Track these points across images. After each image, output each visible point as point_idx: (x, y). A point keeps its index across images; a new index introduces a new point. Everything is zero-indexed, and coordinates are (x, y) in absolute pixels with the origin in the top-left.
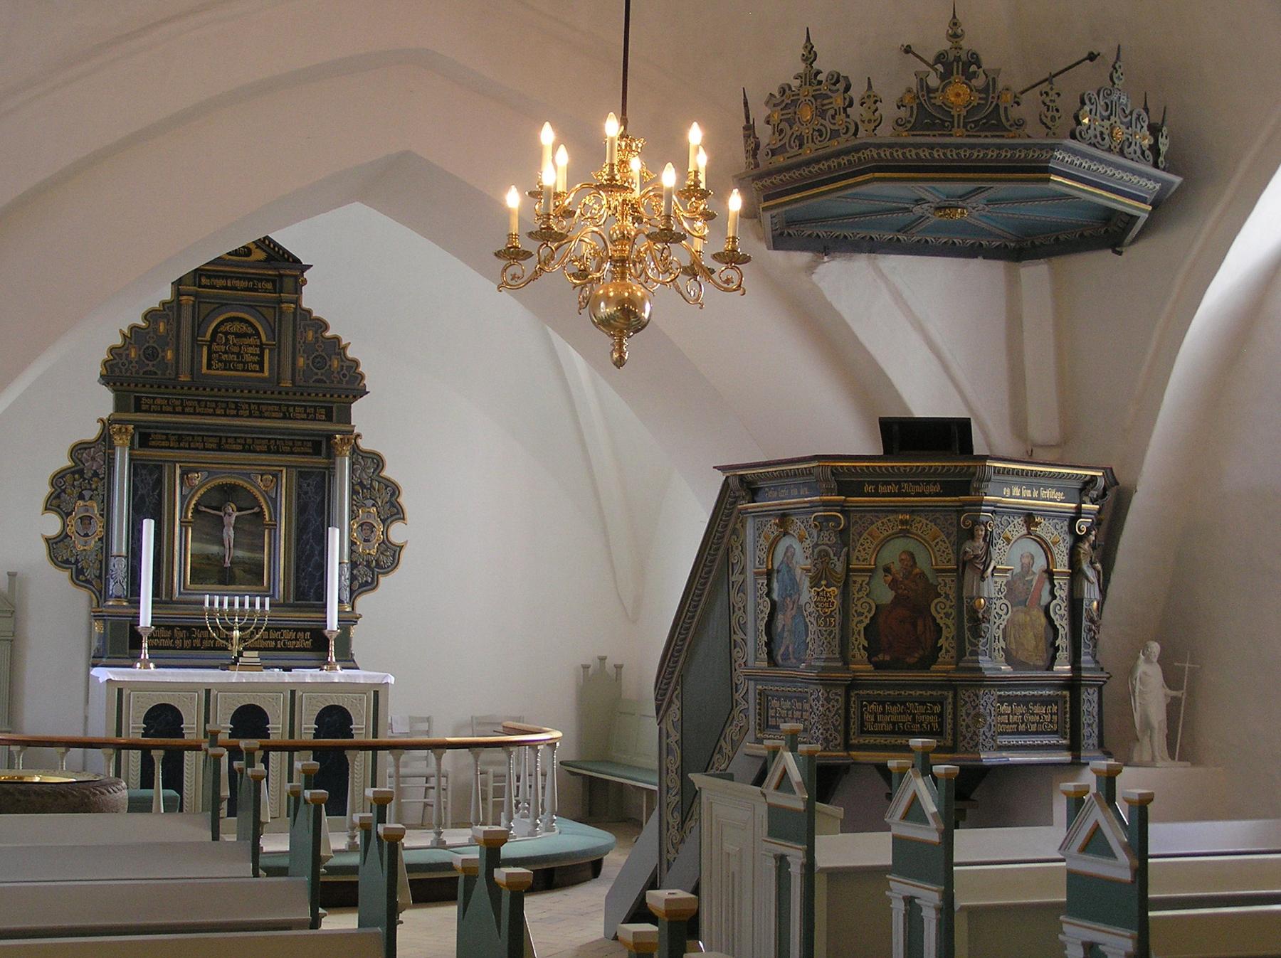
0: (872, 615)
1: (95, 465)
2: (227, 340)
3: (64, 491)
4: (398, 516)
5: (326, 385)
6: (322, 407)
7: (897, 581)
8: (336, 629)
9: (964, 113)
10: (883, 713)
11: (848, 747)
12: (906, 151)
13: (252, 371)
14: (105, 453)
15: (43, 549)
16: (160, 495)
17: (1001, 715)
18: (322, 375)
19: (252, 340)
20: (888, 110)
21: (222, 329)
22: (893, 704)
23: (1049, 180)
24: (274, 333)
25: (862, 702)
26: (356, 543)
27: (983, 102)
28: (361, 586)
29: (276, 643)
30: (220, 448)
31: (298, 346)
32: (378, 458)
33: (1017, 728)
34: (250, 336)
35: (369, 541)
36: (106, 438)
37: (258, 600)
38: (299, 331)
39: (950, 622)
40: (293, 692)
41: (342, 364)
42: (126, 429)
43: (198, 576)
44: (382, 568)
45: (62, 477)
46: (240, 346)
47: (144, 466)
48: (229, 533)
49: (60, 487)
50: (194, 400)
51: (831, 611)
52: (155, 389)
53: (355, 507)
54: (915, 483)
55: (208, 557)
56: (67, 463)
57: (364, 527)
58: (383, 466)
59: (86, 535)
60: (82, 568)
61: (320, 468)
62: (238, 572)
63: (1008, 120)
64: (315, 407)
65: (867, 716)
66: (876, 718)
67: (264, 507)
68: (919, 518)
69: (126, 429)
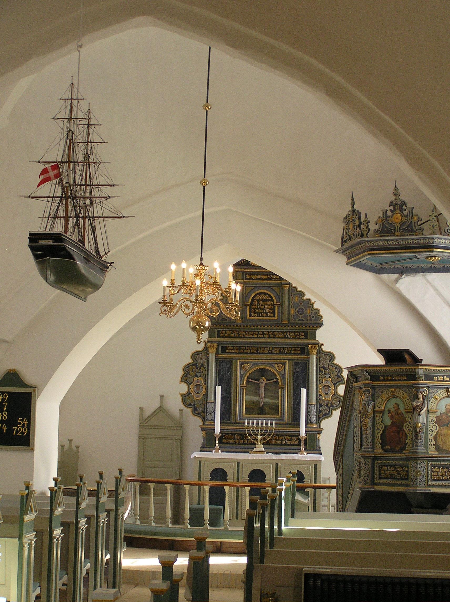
0: (437, 431)
1: (202, 362)
2: (258, 303)
3: (189, 373)
4: (342, 382)
5: (304, 322)
6: (302, 332)
7: (393, 416)
8: (304, 435)
9: (399, 226)
10: (387, 470)
11: (373, 484)
12: (378, 242)
13: (270, 317)
14: (206, 356)
15: (180, 399)
16: (231, 374)
17: (434, 472)
18: (300, 317)
19: (270, 303)
20: (373, 227)
21: (256, 298)
22: (391, 466)
23: (433, 251)
24: (280, 298)
25: (380, 465)
26: (321, 395)
27: (406, 221)
28: (324, 415)
29: (282, 442)
30: (257, 352)
31: (291, 304)
32: (332, 355)
33: (442, 478)
34: (269, 300)
35: (327, 394)
36: (206, 349)
37: (269, 421)
38: (291, 297)
39: (410, 433)
40: (277, 464)
41: (312, 311)
42: (213, 345)
43: (249, 411)
44: (333, 407)
45: (188, 367)
46: (264, 306)
47: (224, 362)
48: (262, 391)
49: (187, 372)
50: (243, 331)
51: (367, 428)
52: (225, 327)
53: (320, 378)
54: (398, 376)
55: (253, 402)
56: (190, 361)
57: (325, 387)
58: (334, 358)
59: (198, 393)
60: (197, 407)
61: (304, 360)
62: (267, 409)
63: (415, 228)
64: (299, 332)
65: (382, 471)
66: (385, 472)
67: (279, 379)
68: (399, 390)
69: (213, 345)
